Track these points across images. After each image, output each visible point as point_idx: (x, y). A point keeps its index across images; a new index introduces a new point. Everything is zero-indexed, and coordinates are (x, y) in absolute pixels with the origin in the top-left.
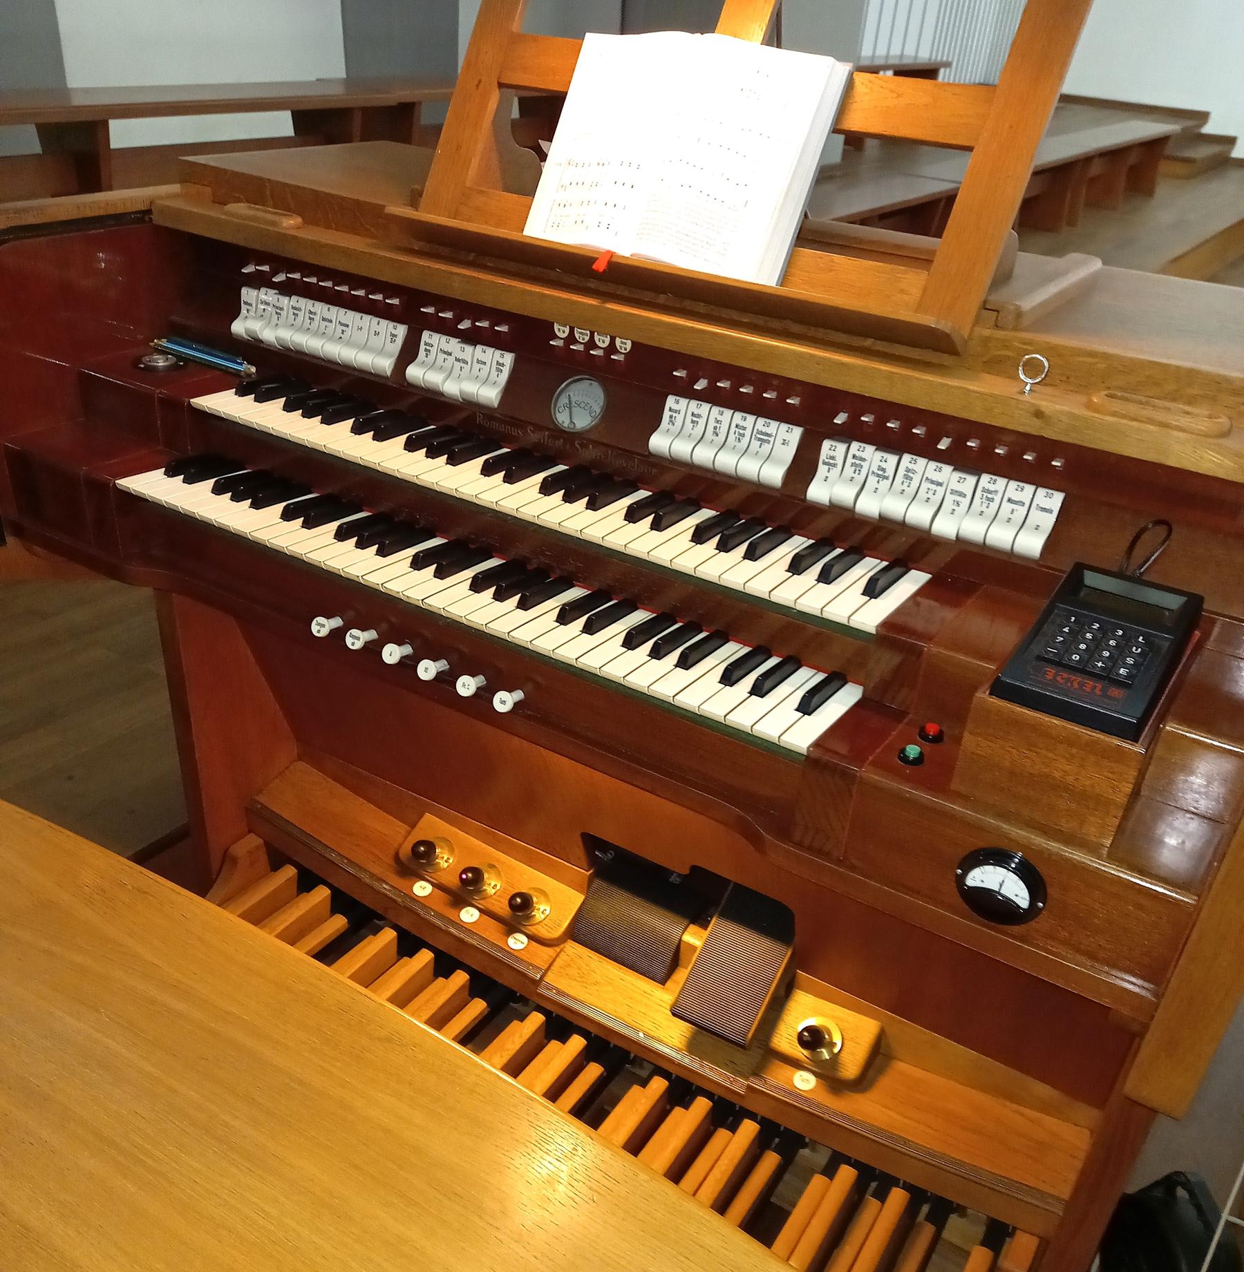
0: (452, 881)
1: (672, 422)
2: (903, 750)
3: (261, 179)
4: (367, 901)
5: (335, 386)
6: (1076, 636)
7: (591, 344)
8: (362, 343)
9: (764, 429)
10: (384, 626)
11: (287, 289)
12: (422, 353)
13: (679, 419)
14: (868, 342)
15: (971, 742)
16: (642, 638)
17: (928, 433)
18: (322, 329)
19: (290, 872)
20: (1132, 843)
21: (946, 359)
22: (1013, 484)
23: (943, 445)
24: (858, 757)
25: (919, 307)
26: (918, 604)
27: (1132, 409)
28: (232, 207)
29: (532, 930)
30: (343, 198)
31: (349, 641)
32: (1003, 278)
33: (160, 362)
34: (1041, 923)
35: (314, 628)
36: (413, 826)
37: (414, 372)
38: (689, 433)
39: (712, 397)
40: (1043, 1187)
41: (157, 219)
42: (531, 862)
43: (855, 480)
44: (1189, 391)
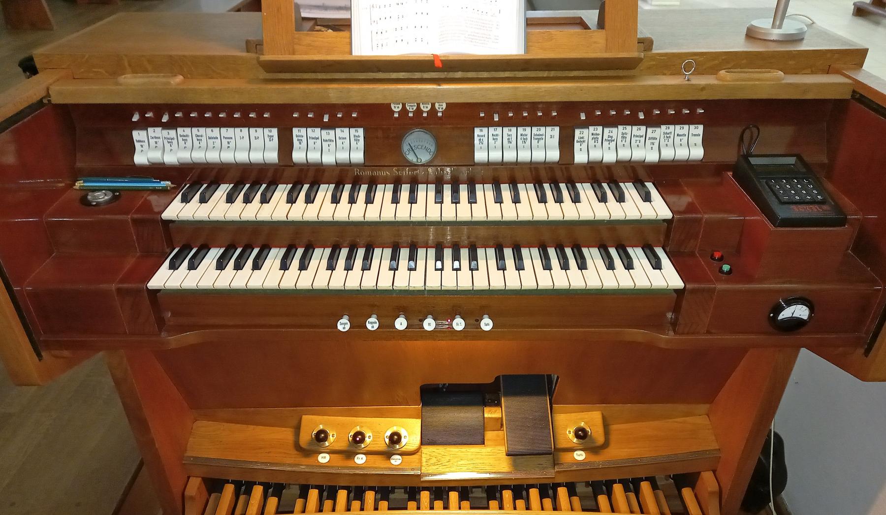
1: (300, 141)
8: (256, 146)
16: (179, 262)
17: (681, 111)
22: (678, 127)
23: (165, 119)
25: (607, 49)
38: (492, 145)
39: (505, 123)
43: (595, 146)
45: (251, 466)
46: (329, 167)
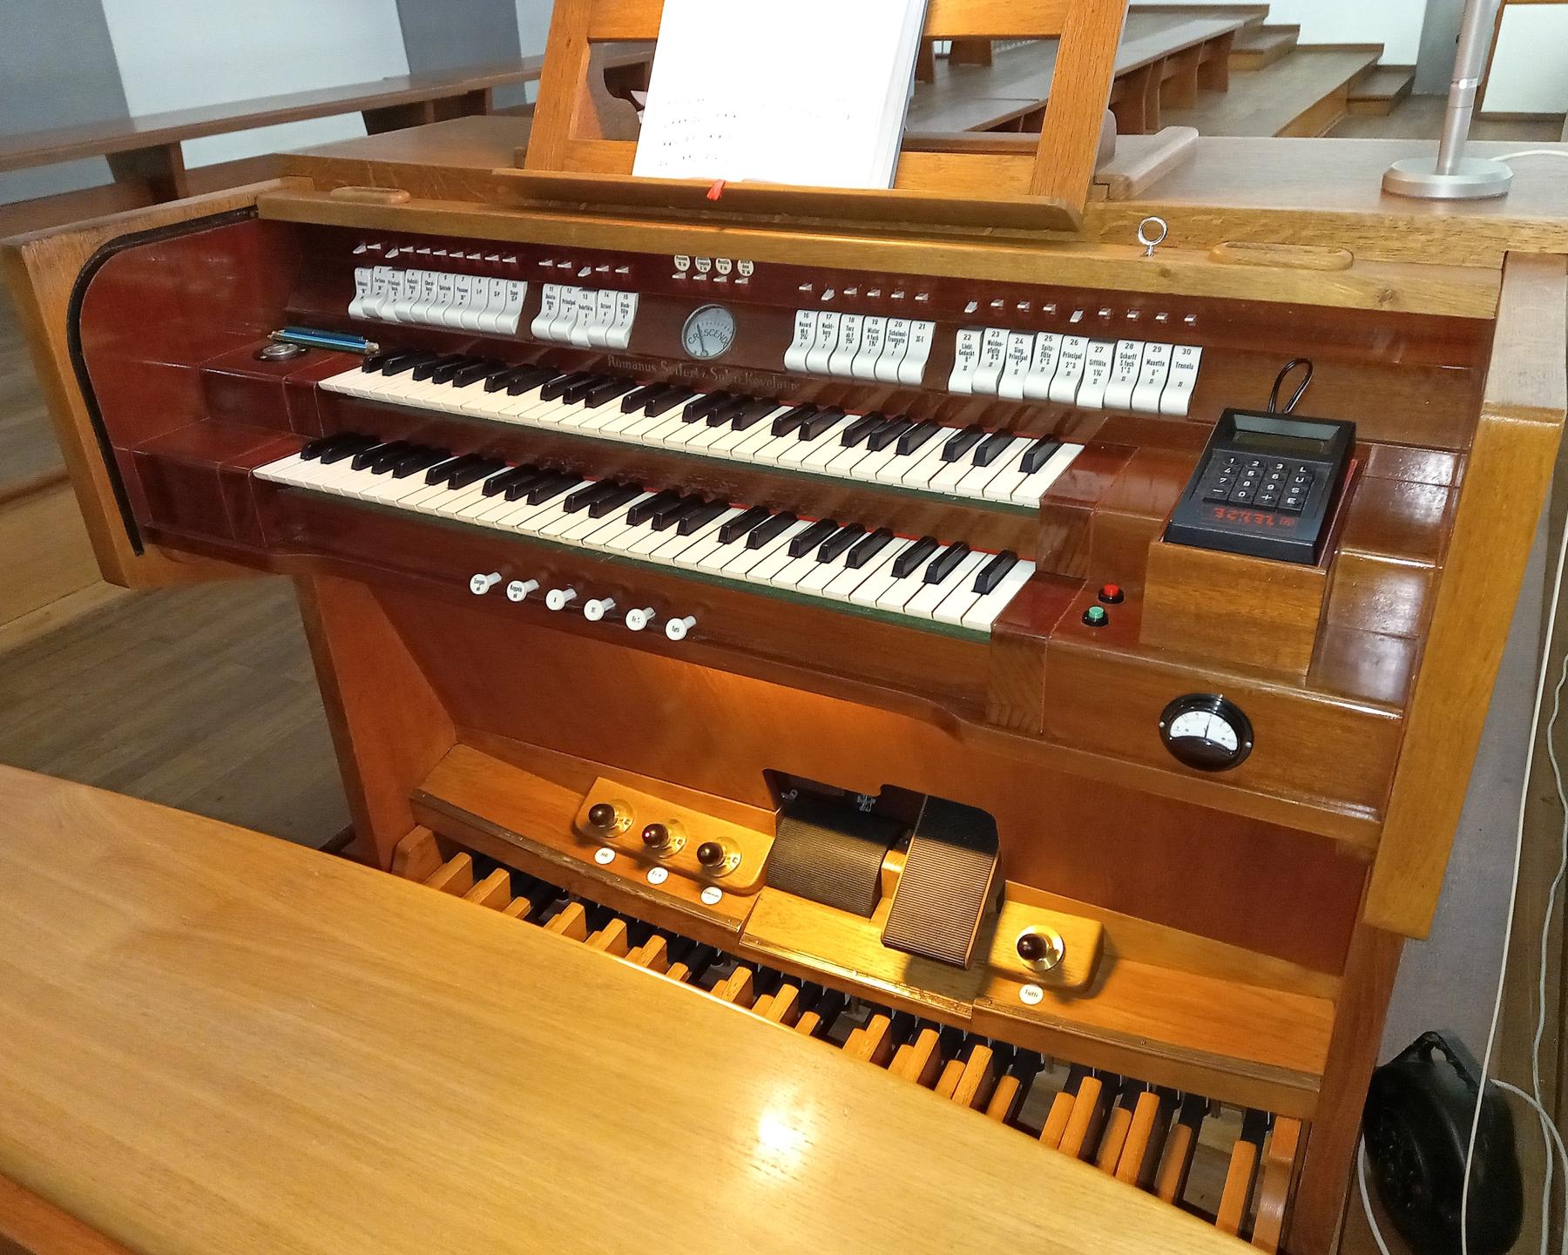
0: (635, 842)
2: (1087, 613)
3: (361, 163)
4: (550, 878)
5: (462, 350)
6: (1238, 474)
7: (714, 273)
8: (486, 306)
9: (897, 329)
10: (544, 575)
11: (401, 264)
12: (545, 306)
13: (811, 331)
14: (987, 232)
15: (1153, 591)
17: (1059, 310)
18: (441, 298)
19: (463, 860)
20: (1332, 658)
21: (1064, 236)
23: (1076, 318)
24: (1044, 628)
26: (1073, 478)
27: (1253, 255)
28: (337, 192)
29: (725, 881)
30: (446, 169)
31: (510, 594)
32: (1107, 156)
33: (282, 351)
34: (1248, 765)
35: (474, 587)
36: (586, 794)
37: (539, 326)
38: (822, 344)
39: (840, 306)
40: (1297, 1067)
41: (263, 214)
42: (714, 811)
43: (992, 365)
44: (1305, 233)
45: (495, 832)
46: (1008, 404)
